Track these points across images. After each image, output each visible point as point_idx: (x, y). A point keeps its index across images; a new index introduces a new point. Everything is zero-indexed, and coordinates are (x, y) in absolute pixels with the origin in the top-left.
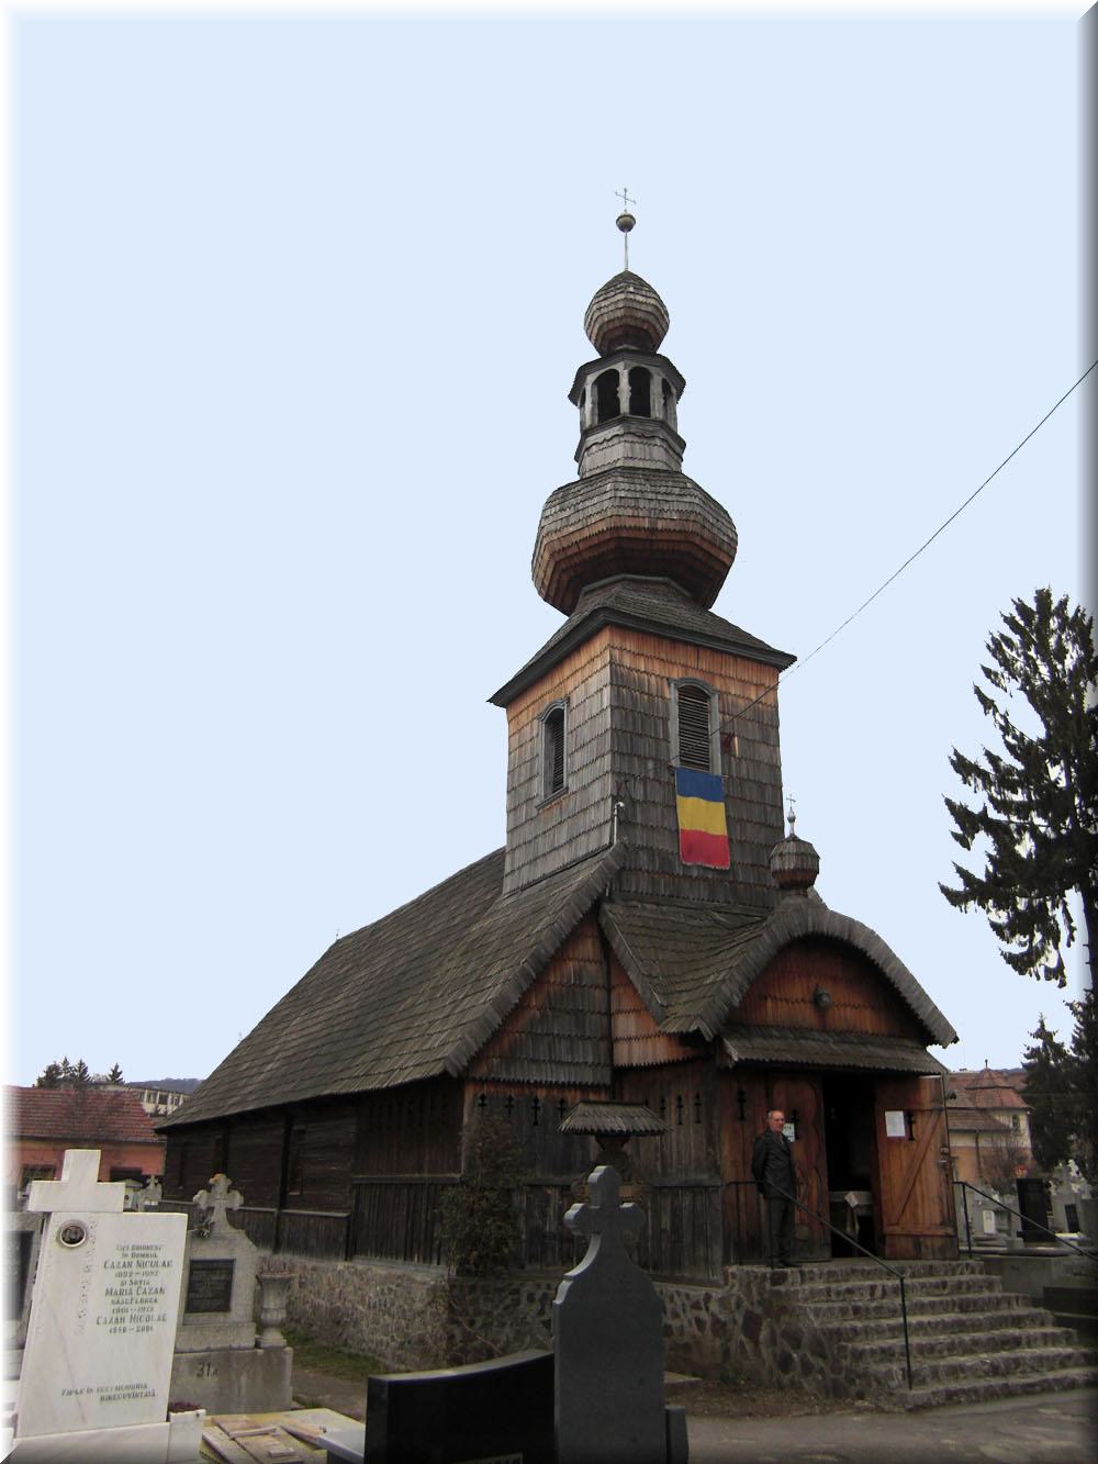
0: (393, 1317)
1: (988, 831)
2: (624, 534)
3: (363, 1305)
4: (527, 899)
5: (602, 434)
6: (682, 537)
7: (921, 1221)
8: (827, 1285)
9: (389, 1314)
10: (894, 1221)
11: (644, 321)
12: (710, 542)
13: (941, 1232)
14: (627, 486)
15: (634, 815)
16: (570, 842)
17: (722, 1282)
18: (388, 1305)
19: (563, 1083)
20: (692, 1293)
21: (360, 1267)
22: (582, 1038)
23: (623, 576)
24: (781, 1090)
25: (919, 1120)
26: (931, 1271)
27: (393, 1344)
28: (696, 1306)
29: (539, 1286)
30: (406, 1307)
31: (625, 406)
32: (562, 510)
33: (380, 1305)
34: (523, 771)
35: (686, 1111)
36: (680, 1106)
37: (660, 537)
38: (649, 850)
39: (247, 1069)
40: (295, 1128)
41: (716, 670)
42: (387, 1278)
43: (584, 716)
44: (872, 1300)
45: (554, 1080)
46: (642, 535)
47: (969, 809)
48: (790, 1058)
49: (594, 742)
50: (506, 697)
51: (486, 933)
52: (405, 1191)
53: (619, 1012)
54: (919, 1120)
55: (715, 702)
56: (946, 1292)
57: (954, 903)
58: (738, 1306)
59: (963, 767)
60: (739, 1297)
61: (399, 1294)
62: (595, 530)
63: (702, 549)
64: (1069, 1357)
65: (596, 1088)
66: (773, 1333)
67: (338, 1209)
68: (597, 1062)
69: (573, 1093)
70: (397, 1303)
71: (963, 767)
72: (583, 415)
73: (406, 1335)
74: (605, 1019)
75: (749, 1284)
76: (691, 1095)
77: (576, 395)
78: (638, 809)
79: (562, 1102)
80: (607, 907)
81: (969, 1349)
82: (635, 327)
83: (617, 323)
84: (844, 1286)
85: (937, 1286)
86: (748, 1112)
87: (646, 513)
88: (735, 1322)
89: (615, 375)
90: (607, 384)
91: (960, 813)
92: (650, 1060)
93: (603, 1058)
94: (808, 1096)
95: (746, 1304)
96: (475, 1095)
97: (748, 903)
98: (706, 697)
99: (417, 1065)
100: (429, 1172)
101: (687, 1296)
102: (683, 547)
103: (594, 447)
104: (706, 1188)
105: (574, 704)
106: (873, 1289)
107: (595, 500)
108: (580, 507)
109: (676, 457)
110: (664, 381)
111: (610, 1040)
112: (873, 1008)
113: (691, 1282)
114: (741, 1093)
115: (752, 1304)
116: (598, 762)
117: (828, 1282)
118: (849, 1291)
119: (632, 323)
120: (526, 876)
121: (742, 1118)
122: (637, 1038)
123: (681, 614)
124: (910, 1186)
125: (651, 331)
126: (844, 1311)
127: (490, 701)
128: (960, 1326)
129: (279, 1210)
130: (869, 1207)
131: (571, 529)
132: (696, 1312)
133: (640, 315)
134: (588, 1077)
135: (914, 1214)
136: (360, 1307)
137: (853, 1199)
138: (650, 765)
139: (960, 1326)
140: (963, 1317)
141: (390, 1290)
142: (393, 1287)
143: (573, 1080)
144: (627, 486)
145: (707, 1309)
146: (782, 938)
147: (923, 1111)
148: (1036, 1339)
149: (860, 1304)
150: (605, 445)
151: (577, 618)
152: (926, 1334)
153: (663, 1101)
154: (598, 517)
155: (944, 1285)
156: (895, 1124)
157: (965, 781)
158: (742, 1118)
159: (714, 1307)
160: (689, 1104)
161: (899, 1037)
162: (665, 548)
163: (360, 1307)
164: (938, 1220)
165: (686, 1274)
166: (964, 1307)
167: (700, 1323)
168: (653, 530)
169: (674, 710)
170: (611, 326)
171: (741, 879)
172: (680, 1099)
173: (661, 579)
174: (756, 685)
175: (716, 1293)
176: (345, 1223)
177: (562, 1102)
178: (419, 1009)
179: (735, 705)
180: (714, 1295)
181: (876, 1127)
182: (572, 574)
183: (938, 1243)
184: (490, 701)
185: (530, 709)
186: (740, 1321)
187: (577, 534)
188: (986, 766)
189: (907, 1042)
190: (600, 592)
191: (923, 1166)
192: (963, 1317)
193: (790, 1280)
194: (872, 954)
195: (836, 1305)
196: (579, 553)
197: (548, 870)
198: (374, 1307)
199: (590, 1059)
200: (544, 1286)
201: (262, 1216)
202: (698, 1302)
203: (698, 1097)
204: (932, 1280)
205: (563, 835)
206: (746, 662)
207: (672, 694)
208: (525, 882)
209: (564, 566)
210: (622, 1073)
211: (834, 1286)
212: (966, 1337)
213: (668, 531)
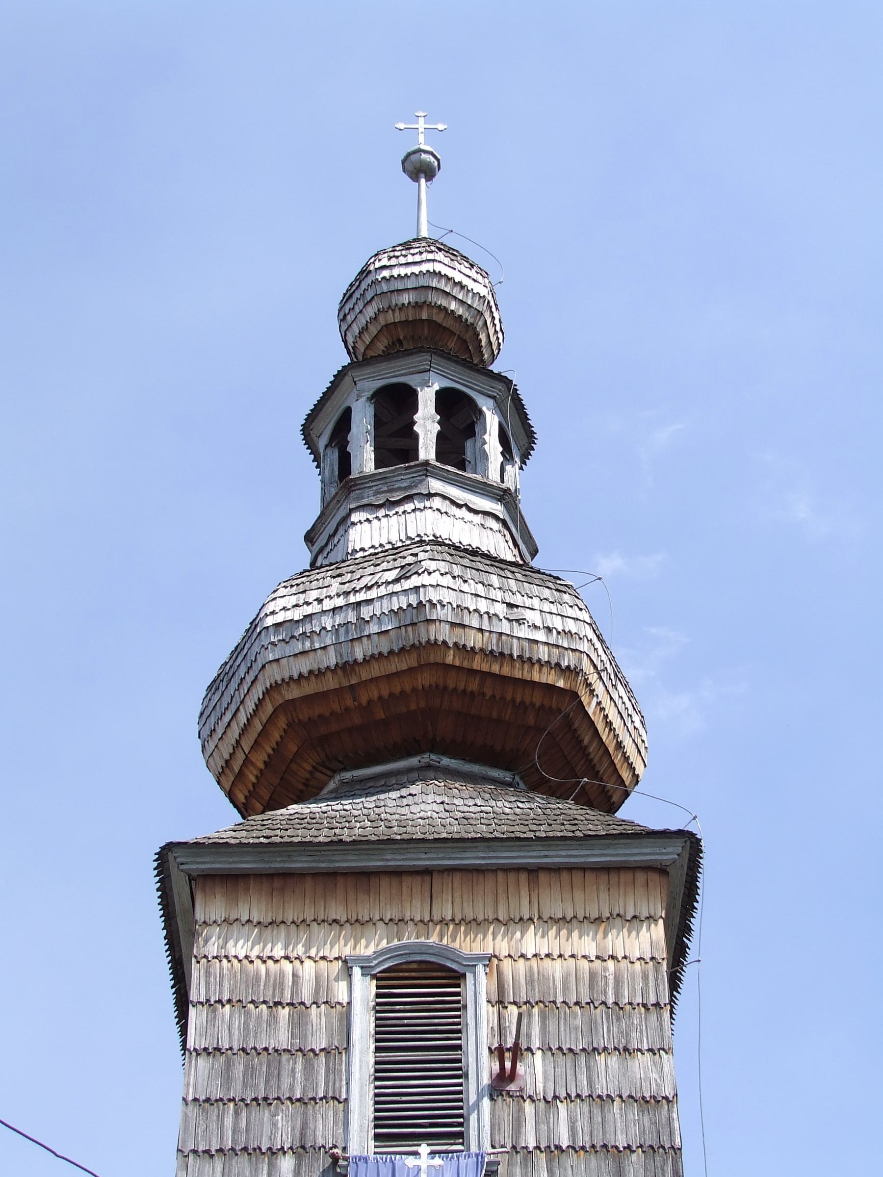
2: (294, 693)
6: (412, 661)
11: (418, 306)
31: (427, 451)
37: (365, 675)
46: (331, 683)
47: (501, 449)
55: (478, 987)
63: (472, 672)
81: (493, 318)
82: (405, 323)
83: (374, 330)
98: (456, 978)
102: (425, 679)
119: (398, 317)
123: (591, 821)
125: (439, 318)
133: (405, 299)
151: (242, 836)
168: (347, 667)
169: (363, 1025)
170: (367, 339)
196: (247, 761)
206: (614, 878)
207: (364, 990)
209: (241, 798)
213: (379, 657)
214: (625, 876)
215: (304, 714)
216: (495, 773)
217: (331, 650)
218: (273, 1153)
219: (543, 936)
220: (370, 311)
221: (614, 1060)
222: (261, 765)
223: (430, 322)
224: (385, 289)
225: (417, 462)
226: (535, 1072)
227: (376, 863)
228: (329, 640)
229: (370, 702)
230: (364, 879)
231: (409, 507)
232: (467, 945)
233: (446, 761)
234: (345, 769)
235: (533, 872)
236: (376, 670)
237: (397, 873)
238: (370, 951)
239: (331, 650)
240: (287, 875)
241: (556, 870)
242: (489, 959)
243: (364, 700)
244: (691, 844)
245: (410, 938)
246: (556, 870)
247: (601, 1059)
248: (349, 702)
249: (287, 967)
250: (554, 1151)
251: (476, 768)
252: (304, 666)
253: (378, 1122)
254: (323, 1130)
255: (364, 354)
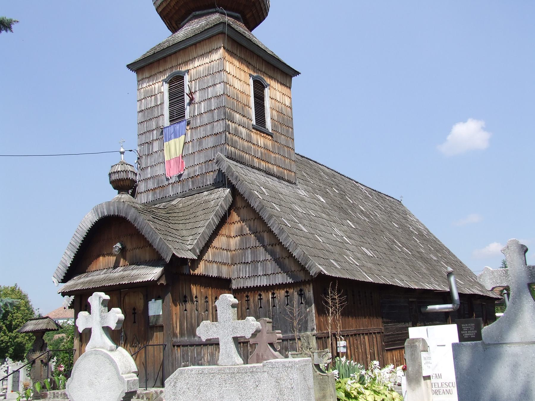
55: (187, 78)
98: (182, 78)
214: (214, 38)
216: (211, 10)
218: (153, 130)
219: (62, 261)
225: (247, 33)
226: (197, 97)
227: (165, 55)
230: (165, 59)
232: (184, 69)
233: (197, 13)
235: (195, 44)
237: (170, 55)
238: (165, 78)
240: (151, 63)
241: (199, 42)
242: (188, 71)
244: (233, 338)
245: (174, 71)
246: (199, 42)
249: (153, 86)
251: (205, 11)
253: (170, 118)
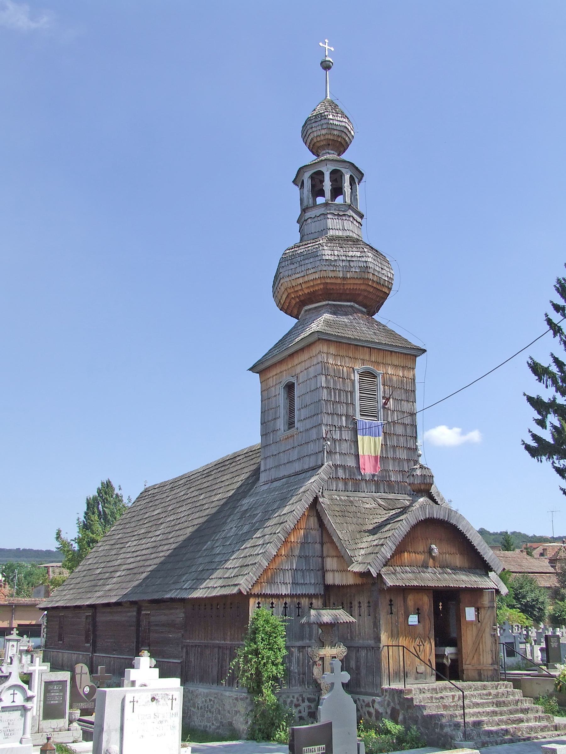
0: (213, 713)
1: (555, 412)
3: (195, 708)
4: (275, 490)
5: (313, 212)
7: (482, 662)
8: (431, 695)
9: (210, 712)
10: (468, 662)
11: (338, 136)
12: (377, 283)
13: (492, 668)
14: (330, 252)
15: (335, 448)
16: (299, 459)
17: (380, 694)
18: (210, 708)
19: (299, 594)
20: (366, 700)
21: (191, 689)
22: (310, 570)
23: (327, 302)
24: (411, 600)
25: (482, 612)
26: (484, 688)
27: (213, 727)
28: (368, 705)
29: (288, 697)
30: (220, 708)
32: (292, 263)
33: (205, 708)
34: (271, 414)
35: (363, 609)
36: (360, 607)
38: (344, 467)
39: (100, 573)
40: (143, 612)
41: (380, 360)
42: (207, 695)
43: (306, 389)
44: (453, 702)
45: (294, 593)
46: (339, 281)
48: (416, 584)
49: (313, 406)
50: (261, 369)
51: (252, 508)
52: (216, 650)
53: (328, 556)
54: (482, 612)
56: (490, 697)
57: (533, 456)
58: (388, 705)
59: (537, 370)
60: (389, 701)
61: (216, 702)
62: (311, 277)
64: (546, 727)
65: (315, 596)
66: (404, 718)
67: (175, 657)
68: (316, 582)
69: (304, 599)
70: (215, 706)
71: (537, 370)
72: (302, 194)
73: (221, 722)
74: (320, 559)
75: (394, 695)
76: (366, 601)
77: (298, 181)
78: (337, 443)
79: (299, 604)
80: (321, 500)
83: (322, 138)
84: (439, 695)
85: (486, 695)
86: (394, 610)
87: (341, 269)
88: (387, 713)
89: (321, 173)
90: (317, 177)
91: (536, 403)
92: (345, 583)
93: (320, 580)
94: (426, 601)
95: (392, 704)
96: (255, 602)
97: (397, 492)
98: (375, 377)
99: (222, 587)
100: (231, 640)
101: (364, 701)
102: (363, 287)
103: (309, 220)
104: (373, 648)
105: (301, 381)
106: (453, 697)
107: (311, 260)
108: (302, 263)
109: (357, 225)
110: (351, 177)
111: (323, 571)
112: (461, 554)
113: (366, 694)
114: (391, 601)
115: (395, 704)
116: (315, 417)
117: (432, 693)
118: (442, 698)
119: (332, 138)
120: (274, 474)
121: (391, 613)
122: (337, 571)
124: (476, 646)
125: (343, 142)
126: (438, 707)
127: (250, 370)
128: (494, 713)
129: (92, 654)
130: (456, 654)
131: (298, 276)
132: (368, 709)
133: (336, 133)
134: (312, 591)
135: (479, 659)
136: (193, 709)
137: (449, 651)
138: (344, 418)
139: (494, 713)
140: (497, 709)
141: (210, 700)
142: (213, 699)
143: (304, 593)
144: (330, 252)
145: (373, 707)
146: (413, 522)
147: (484, 608)
148: (531, 719)
149: (447, 704)
150: (316, 219)
152: (477, 717)
153: (351, 603)
154: (313, 271)
155: (490, 694)
156: (470, 613)
157: (540, 380)
158: (391, 613)
159: (376, 706)
160: (364, 606)
161: (474, 569)
162: (352, 288)
163: (193, 709)
164: (490, 661)
165: (362, 690)
166: (498, 704)
167: (370, 714)
171: (393, 479)
172: (360, 603)
173: (349, 304)
174: (403, 367)
175: (378, 699)
176: (180, 666)
177: (299, 604)
178: (217, 551)
179: (391, 380)
180: (376, 700)
181: (460, 615)
182: (298, 300)
183: (490, 673)
184: (250, 370)
185: (274, 377)
186: (389, 712)
187: (301, 279)
188: (554, 369)
189: (478, 571)
190: (314, 311)
191: (484, 635)
192: (497, 709)
193: (413, 692)
194: (460, 527)
195: (435, 704)
197: (286, 473)
198: (201, 708)
199: (313, 582)
200: (291, 697)
201: (123, 661)
202: (369, 703)
203: (369, 602)
204: (485, 692)
205: (294, 455)
207: (357, 377)
208: (273, 478)
210: (328, 588)
211: (435, 695)
212: (496, 718)
215: (329, 287)
217: (341, 272)
220: (324, 132)
221: (405, 403)
222: (306, 292)
223: (341, 143)
224: (330, 127)
228: (341, 269)
229: (347, 288)
231: (344, 218)
234: (329, 300)
236: (352, 281)
239: (341, 272)
243: (346, 288)
247: (403, 402)
248: (342, 287)
250: (394, 422)
252: (331, 274)
254: (351, 413)
255: (315, 143)
